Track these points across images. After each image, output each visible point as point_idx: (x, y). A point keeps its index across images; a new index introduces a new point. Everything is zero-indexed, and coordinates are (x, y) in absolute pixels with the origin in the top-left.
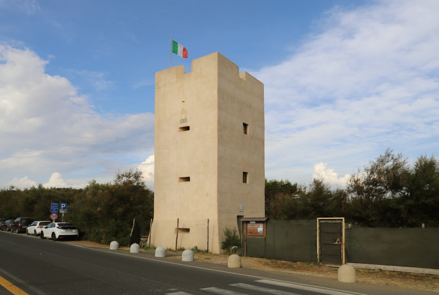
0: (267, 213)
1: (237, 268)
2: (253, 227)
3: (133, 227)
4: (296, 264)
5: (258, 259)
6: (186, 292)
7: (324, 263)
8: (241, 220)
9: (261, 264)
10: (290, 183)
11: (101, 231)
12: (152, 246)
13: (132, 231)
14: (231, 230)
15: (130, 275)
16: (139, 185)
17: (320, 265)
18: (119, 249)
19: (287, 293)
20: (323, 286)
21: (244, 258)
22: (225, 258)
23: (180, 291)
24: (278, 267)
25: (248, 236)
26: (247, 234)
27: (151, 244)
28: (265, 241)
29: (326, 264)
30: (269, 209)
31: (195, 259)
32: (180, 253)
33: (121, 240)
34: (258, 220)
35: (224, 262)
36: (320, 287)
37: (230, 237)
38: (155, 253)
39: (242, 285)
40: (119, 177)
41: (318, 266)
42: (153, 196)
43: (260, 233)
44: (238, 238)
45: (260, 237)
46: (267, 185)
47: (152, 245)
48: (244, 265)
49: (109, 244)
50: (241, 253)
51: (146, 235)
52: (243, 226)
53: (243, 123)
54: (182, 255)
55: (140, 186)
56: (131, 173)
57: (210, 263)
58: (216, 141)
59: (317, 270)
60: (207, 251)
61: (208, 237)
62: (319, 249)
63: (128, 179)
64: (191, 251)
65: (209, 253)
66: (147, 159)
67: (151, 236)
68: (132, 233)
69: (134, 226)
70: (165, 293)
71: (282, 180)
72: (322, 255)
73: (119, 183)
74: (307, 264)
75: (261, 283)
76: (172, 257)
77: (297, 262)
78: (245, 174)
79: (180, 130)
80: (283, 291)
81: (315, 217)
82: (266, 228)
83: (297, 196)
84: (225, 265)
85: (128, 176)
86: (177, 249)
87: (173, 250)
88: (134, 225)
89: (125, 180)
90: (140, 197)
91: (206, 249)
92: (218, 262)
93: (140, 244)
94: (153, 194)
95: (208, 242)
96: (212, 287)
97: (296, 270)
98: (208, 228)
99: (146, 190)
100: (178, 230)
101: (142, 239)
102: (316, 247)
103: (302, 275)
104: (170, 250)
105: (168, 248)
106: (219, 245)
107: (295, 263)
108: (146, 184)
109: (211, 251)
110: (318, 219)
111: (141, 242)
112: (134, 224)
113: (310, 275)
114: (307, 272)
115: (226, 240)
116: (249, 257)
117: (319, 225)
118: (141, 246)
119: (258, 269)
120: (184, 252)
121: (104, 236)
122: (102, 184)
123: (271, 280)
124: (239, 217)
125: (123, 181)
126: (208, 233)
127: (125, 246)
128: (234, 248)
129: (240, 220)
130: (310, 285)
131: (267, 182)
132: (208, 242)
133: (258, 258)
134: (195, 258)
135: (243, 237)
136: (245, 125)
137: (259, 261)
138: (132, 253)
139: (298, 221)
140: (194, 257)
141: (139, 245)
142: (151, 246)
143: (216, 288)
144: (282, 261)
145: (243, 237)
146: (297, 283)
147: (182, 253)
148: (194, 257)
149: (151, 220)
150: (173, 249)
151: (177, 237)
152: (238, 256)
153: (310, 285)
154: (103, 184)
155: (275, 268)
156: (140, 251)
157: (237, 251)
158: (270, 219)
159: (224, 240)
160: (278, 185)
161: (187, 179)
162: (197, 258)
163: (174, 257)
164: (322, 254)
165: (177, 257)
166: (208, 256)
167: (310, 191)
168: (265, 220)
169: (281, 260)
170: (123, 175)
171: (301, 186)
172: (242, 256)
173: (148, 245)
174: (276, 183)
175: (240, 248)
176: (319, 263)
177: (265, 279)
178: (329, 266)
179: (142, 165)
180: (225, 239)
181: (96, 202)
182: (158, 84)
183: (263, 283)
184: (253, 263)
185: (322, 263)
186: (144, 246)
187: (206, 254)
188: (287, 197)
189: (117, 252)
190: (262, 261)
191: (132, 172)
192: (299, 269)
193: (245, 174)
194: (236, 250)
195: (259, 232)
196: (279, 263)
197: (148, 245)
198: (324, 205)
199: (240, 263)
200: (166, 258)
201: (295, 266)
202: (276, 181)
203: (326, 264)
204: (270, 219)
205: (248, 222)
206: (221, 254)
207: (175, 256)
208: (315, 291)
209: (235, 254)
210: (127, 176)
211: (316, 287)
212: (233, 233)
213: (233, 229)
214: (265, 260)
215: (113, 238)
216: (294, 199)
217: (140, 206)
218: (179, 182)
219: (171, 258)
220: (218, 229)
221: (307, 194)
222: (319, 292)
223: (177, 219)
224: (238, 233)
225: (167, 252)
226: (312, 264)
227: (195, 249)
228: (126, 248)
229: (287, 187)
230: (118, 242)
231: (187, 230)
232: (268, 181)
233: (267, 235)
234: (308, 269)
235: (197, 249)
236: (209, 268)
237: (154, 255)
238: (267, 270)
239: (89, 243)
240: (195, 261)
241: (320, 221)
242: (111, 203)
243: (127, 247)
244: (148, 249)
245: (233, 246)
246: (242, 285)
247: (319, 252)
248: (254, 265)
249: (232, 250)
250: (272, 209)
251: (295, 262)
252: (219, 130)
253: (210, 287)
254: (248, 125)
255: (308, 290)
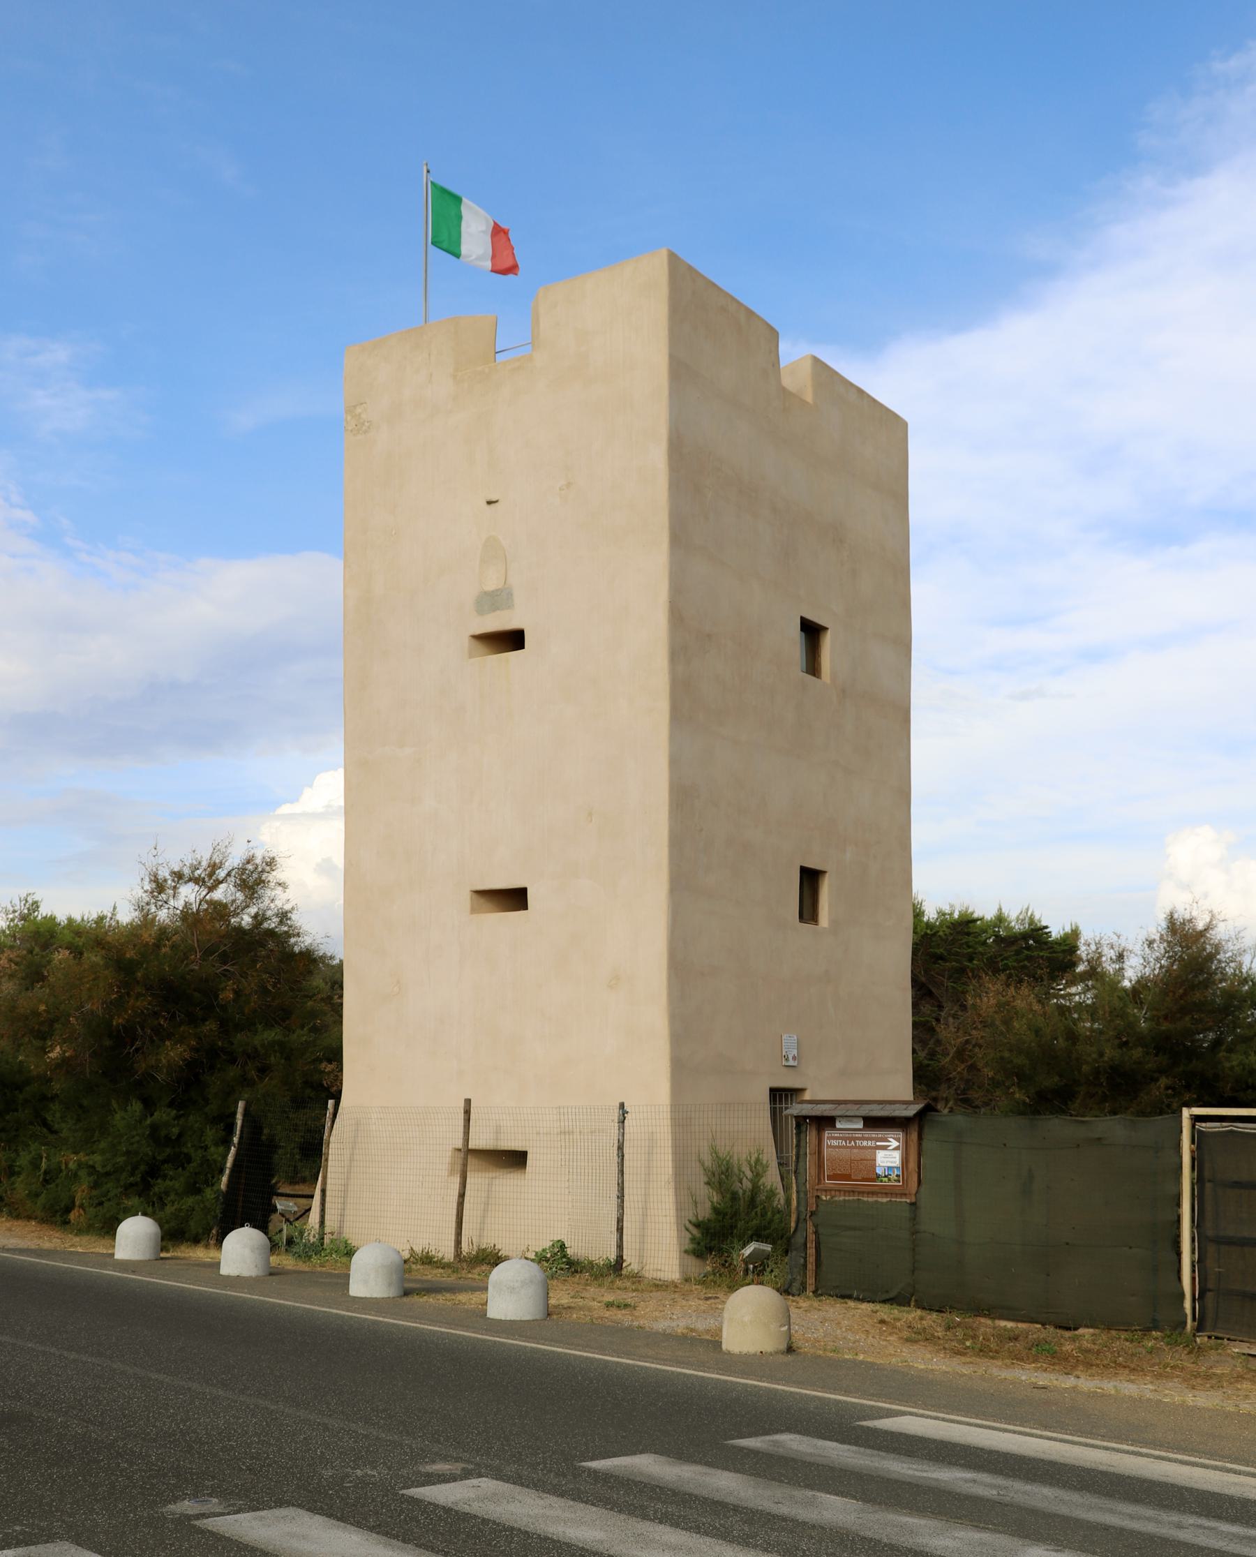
0: (924, 1076)
1: (771, 1354)
2: (852, 1147)
3: (236, 1140)
4: (1073, 1339)
5: (876, 1312)
6: (507, 1479)
7: (1217, 1338)
8: (788, 1112)
9: (891, 1334)
10: (1046, 927)
11: (66, 1164)
12: (332, 1241)
13: (229, 1164)
14: (739, 1160)
15: (221, 1393)
16: (265, 925)
17: (1199, 1348)
18: (163, 1255)
19: (1028, 1487)
20: (1212, 1455)
21: (804, 1304)
22: (708, 1302)
23: (480, 1476)
24: (981, 1351)
25: (826, 1191)
26: (819, 1180)
27: (327, 1230)
28: (914, 1219)
29: (1228, 1339)
30: (932, 1055)
31: (556, 1307)
32: (475, 1274)
33: (173, 1209)
34: (877, 1111)
35: (701, 1325)
36: (1197, 1460)
37: (734, 1197)
38: (348, 1276)
39: (794, 1443)
40: (159, 886)
41: (1190, 1353)
42: (336, 983)
43: (889, 1180)
44: (775, 1203)
45: (885, 1200)
46: (926, 934)
47: (334, 1237)
48: (807, 1341)
49: (109, 1228)
50: (790, 1277)
51: (304, 1180)
52: (802, 1144)
53: (802, 618)
54: (486, 1289)
55: (271, 933)
56: (217, 861)
57: (630, 1329)
58: (664, 705)
59: (1183, 1369)
60: (617, 1266)
61: (621, 1197)
62: (1193, 1266)
63: (204, 893)
64: (535, 1266)
65: (628, 1277)
66: (307, 792)
67: (329, 1187)
68: (227, 1172)
69: (241, 1138)
70: (401, 1489)
71: (1000, 909)
72: (1209, 1295)
73: (163, 915)
74: (1132, 1341)
75: (892, 1433)
76: (439, 1296)
77: (1076, 1329)
78: (810, 878)
79: (480, 647)
80: (1007, 1476)
81: (1175, 1105)
82: (915, 1158)
83: (1078, 994)
84: (708, 1337)
85: (208, 877)
86: (464, 1254)
87: (440, 1261)
88: (238, 1133)
89: (192, 898)
90: (270, 988)
91: (613, 1257)
92: (674, 1324)
93: (271, 1227)
94: (340, 968)
95: (620, 1221)
96: (641, 1453)
97: (1074, 1367)
98: (621, 1148)
99: (301, 953)
100: (466, 1159)
101: (280, 1204)
102: (1179, 1254)
103: (1103, 1396)
104: (427, 1260)
105: (418, 1249)
106: (679, 1237)
107: (1067, 1334)
108: (297, 919)
109: (635, 1267)
110: (1186, 1113)
111: (275, 1218)
112: (242, 1126)
113: (1149, 1395)
114: (1132, 1381)
115: (716, 1210)
116: (831, 1300)
117: (1193, 1142)
118: (276, 1238)
119: (879, 1361)
120: (499, 1274)
121: (81, 1192)
122: (70, 920)
123: (944, 1420)
124: (779, 1095)
125: (180, 904)
126: (621, 1172)
127: (196, 1241)
128: (755, 1248)
129: (785, 1113)
130: (1144, 1450)
131: (925, 919)
132: (620, 1221)
133: (878, 1307)
134: (552, 1302)
135: (802, 1195)
136: (812, 632)
137: (882, 1322)
138: (228, 1277)
139: (1083, 1122)
140: (547, 1297)
141: (266, 1233)
142: (327, 1241)
143: (662, 1459)
144: (1003, 1323)
145: (802, 1195)
146: (1076, 1439)
147: (487, 1276)
148: (547, 1297)
149: (326, 1108)
150: (440, 1255)
151: (462, 1196)
152: (777, 1294)
153: (1144, 1450)
154: (78, 918)
155: (963, 1359)
156: (273, 1265)
157: (769, 1270)
158: (937, 1111)
159: (705, 1213)
160: (980, 935)
161: (516, 898)
162: (565, 1301)
163: (448, 1295)
164: (1210, 1290)
165: (462, 1297)
166: (619, 1292)
167: (1148, 971)
168: (914, 1112)
169: (993, 1319)
170: (178, 876)
171: (1098, 944)
172: (793, 1295)
173: (312, 1236)
174: (971, 925)
175: (787, 1255)
176: (1194, 1336)
177: (911, 1414)
178: (1244, 1354)
179: (278, 824)
180: (708, 1205)
181: (39, 1014)
182: (359, 410)
183: (901, 1434)
184: (849, 1329)
185: (1210, 1337)
186: (290, 1242)
187: (612, 1282)
188: (1024, 998)
189: (150, 1275)
190: (899, 1320)
191: (225, 857)
192: (1089, 1365)
193: (810, 878)
194: (762, 1263)
195: (879, 1171)
196: (982, 1329)
197: (312, 1236)
198: (1217, 1043)
199: (785, 1328)
200: (405, 1299)
201: (1068, 1347)
202: (972, 913)
203: (1233, 1343)
204: (937, 1111)
205: (825, 1122)
206: (687, 1280)
207: (452, 1289)
208: (1170, 1480)
209: (758, 1284)
210: (197, 881)
211: (1176, 1461)
212: (749, 1174)
213: (750, 1153)
214: (912, 1315)
215: (128, 1203)
216: (1062, 1010)
217: (272, 1035)
218: (474, 910)
219: (430, 1300)
220: (675, 1153)
221: (1134, 988)
222: (1196, 1486)
223: (462, 1104)
224: (772, 1178)
225: (410, 1271)
226: (1156, 1339)
227: (556, 1254)
228: (200, 1254)
229: (1029, 948)
230: (161, 1223)
231: (516, 1159)
232: (930, 914)
233: (922, 1189)
234: (1132, 1366)
235: (565, 1256)
236: (628, 1355)
237: (346, 1285)
238: (923, 1367)
239: (8, 1225)
240: (555, 1317)
241: (1199, 1125)
242: (120, 1021)
243: (207, 1246)
244: (310, 1257)
245: (751, 1239)
246: (794, 1443)
247: (1193, 1279)
248: (858, 1341)
249: (743, 1260)
250: (948, 1059)
251: (1068, 1329)
252: (678, 653)
253: (634, 1453)
254: (827, 629)
255: (1133, 1473)
